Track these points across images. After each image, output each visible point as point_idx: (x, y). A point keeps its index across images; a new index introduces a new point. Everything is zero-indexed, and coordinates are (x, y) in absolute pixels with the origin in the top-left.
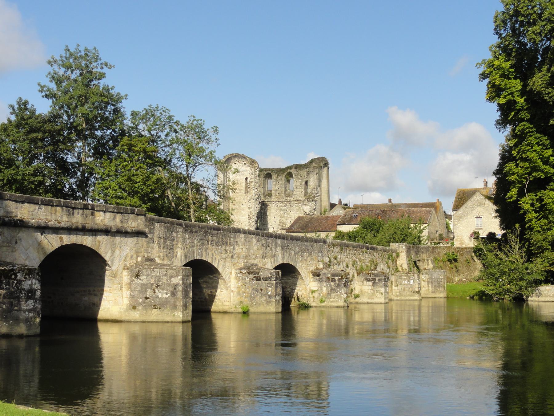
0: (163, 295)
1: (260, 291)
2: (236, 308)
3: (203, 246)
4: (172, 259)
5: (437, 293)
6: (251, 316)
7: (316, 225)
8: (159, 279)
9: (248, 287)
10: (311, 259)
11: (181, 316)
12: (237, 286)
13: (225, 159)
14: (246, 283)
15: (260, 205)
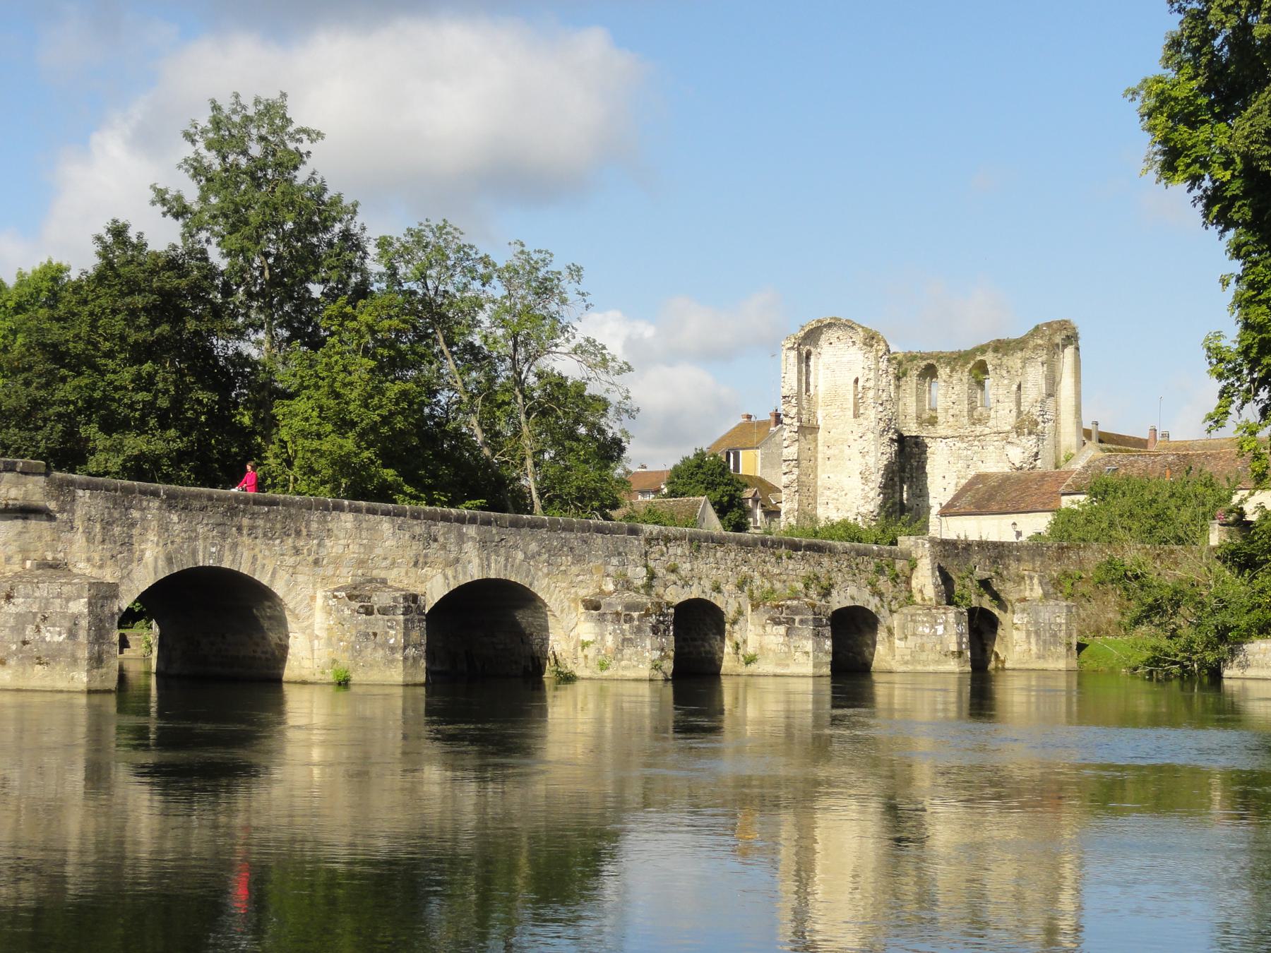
0: (54, 636)
1: (372, 637)
2: (323, 673)
3: (224, 539)
4: (127, 565)
5: (1050, 660)
6: (354, 689)
8: (47, 603)
10: (583, 570)
11: (85, 680)
12: (326, 626)
13: (802, 333)
14: (345, 620)
15: (895, 447)
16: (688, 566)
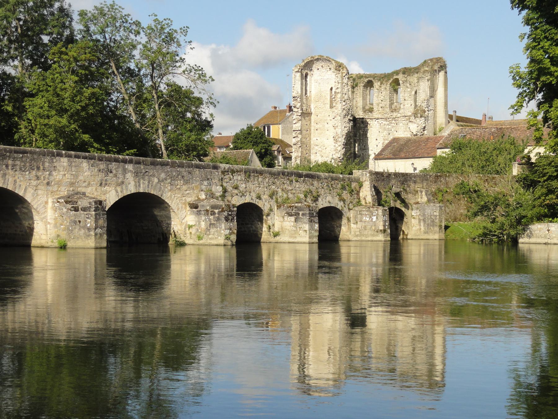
2: (52, 242)
6: (68, 250)
7: (413, 149)
9: (66, 218)
12: (54, 217)
13: (303, 64)
14: (63, 214)
16: (244, 185)
